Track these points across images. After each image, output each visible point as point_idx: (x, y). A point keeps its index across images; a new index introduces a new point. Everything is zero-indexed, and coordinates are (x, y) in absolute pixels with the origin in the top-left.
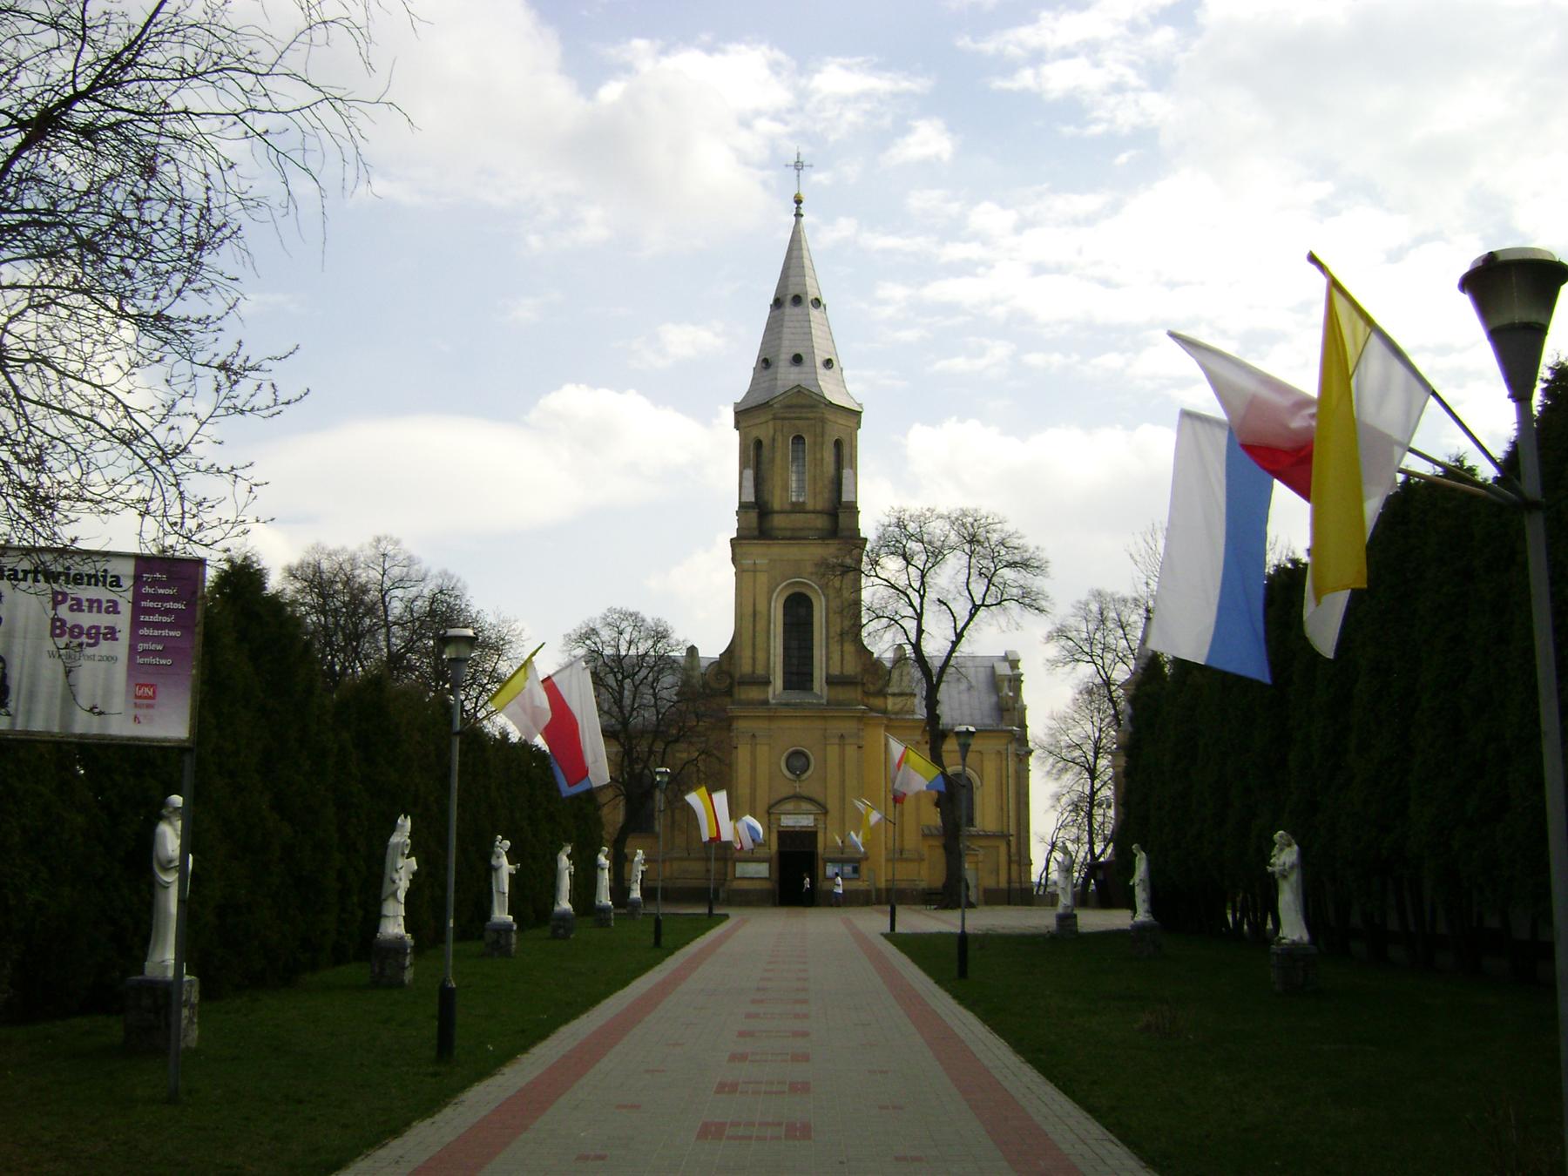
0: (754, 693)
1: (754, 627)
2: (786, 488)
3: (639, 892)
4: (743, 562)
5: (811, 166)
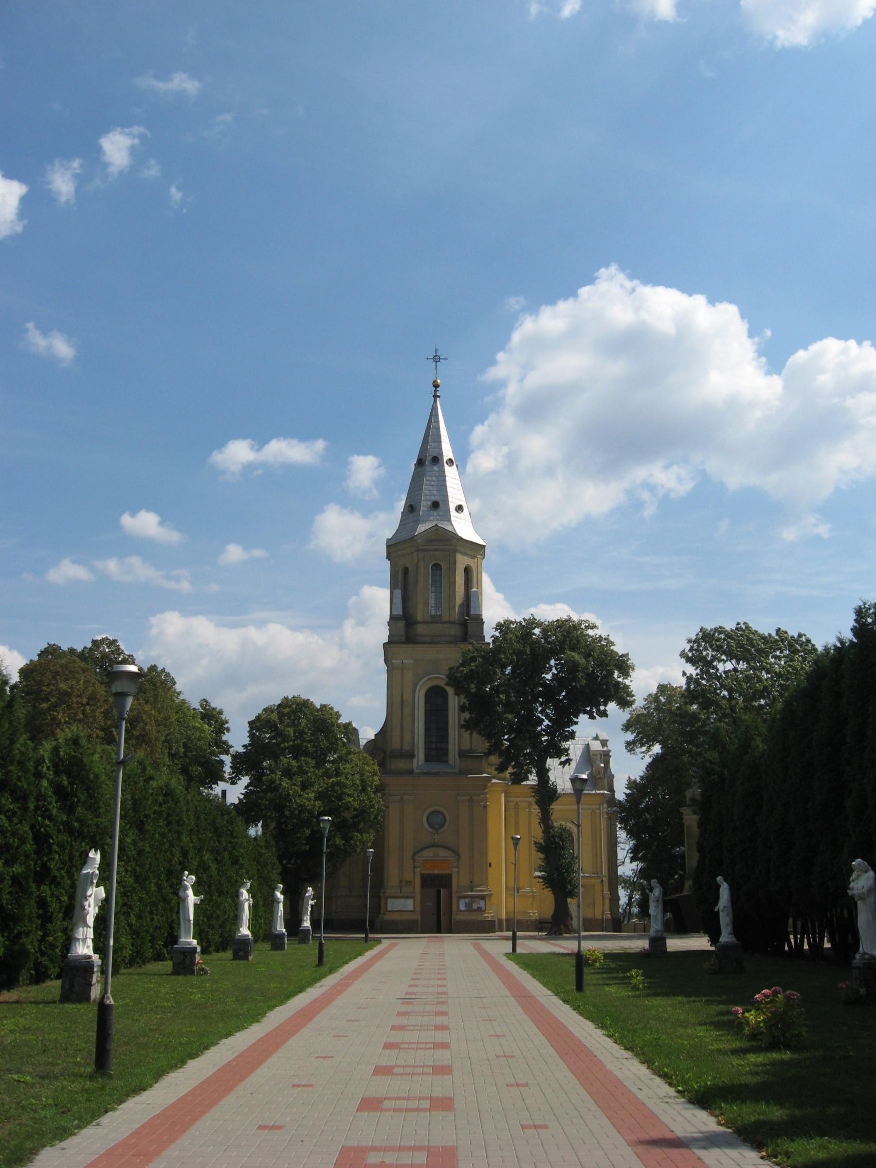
0: (401, 764)
1: (402, 713)
2: (426, 604)
3: (309, 921)
4: (394, 661)
5: (446, 359)
